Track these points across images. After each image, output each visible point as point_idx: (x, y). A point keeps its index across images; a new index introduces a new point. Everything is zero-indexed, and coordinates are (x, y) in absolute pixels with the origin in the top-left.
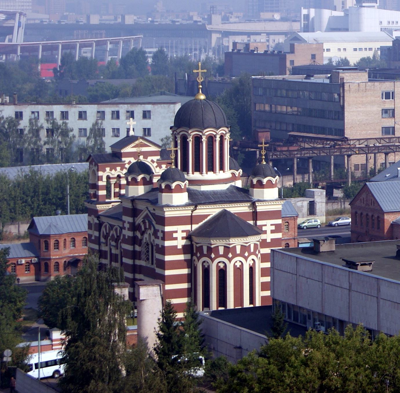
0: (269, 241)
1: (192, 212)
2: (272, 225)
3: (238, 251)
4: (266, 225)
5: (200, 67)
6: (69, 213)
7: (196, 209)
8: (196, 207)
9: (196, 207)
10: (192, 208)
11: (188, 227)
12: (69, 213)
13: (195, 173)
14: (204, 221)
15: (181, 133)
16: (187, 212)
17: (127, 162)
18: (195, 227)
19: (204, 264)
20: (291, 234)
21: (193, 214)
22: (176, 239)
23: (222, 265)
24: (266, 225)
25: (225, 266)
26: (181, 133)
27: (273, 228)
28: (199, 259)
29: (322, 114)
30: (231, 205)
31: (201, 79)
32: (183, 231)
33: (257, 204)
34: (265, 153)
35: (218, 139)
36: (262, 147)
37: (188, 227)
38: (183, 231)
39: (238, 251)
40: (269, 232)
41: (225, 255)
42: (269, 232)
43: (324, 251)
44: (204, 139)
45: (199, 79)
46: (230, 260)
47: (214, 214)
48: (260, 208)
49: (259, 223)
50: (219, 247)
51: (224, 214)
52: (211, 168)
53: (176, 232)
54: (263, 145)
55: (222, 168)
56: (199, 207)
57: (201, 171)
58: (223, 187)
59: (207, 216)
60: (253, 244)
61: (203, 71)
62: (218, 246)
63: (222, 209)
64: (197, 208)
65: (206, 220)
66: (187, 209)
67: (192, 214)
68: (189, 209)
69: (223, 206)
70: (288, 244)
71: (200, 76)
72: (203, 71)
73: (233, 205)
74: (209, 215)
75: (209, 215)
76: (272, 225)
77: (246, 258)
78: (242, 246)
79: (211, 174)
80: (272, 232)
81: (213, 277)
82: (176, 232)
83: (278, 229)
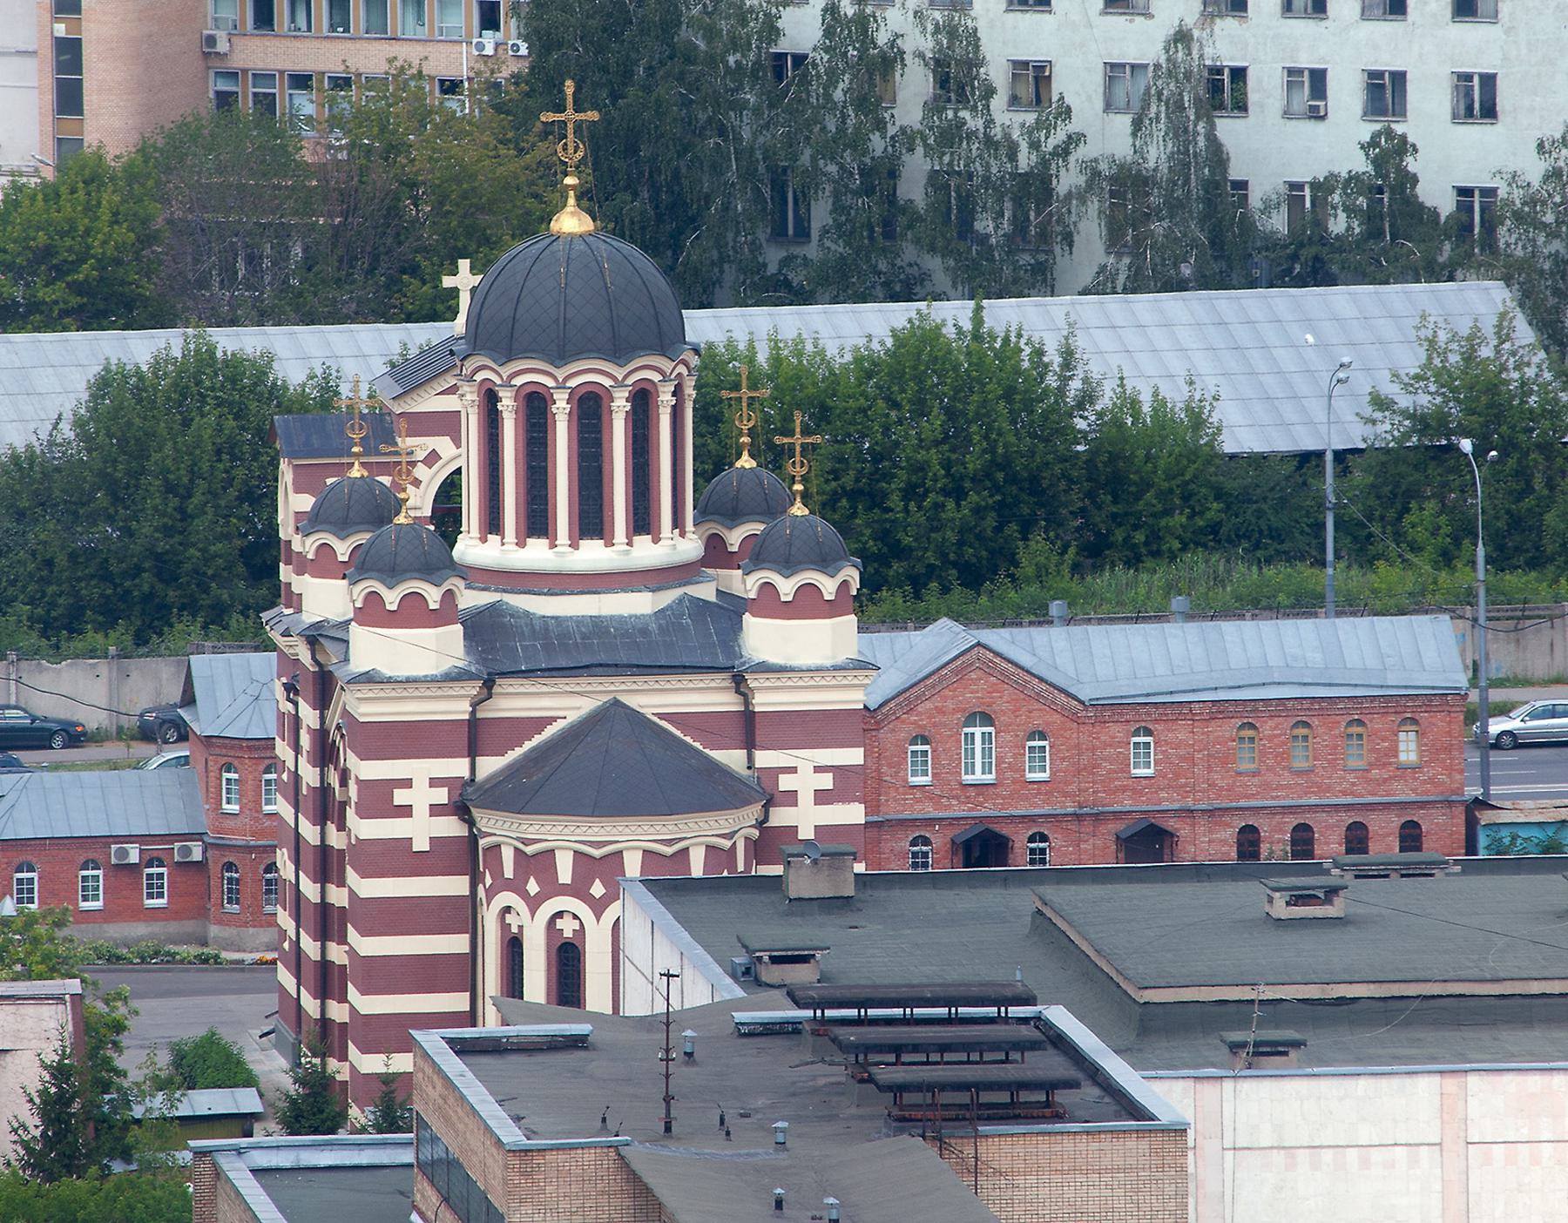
0: (807, 833)
1: (475, 705)
2: (818, 769)
3: (565, 875)
4: (793, 770)
5: (570, 100)
6: (1329, 457)
7: (490, 696)
8: (490, 688)
9: (489, 684)
10: (473, 689)
11: (458, 767)
12: (1329, 457)
13: (584, 543)
14: (528, 745)
15: (479, 377)
16: (455, 707)
17: (420, 455)
18: (489, 765)
19: (509, 918)
20: (1431, 780)
21: (479, 715)
22: (406, 811)
23: (567, 927)
24: (793, 770)
25: (581, 932)
26: (479, 377)
27: (826, 782)
28: (534, 904)
29: (1053, 287)
30: (641, 682)
31: (576, 149)
32: (435, 782)
33: (752, 684)
34: (805, 470)
35: (620, 405)
36: (791, 447)
37: (458, 767)
38: (435, 782)
39: (565, 875)
40: (806, 798)
41: (578, 889)
42: (806, 798)
43: (806, 896)
44: (561, 407)
45: (565, 149)
46: (599, 907)
47: (573, 717)
48: (767, 700)
49: (764, 759)
50: (625, 854)
51: (614, 712)
52: (591, 523)
53: (407, 783)
54: (798, 440)
55: (643, 522)
56: (504, 686)
57: (606, 531)
58: (639, 604)
59: (541, 723)
60: (702, 850)
61: (581, 116)
62: (552, 851)
63: (605, 698)
64: (496, 689)
65: (537, 740)
66: (451, 692)
67: (473, 713)
68: (462, 692)
69: (612, 688)
70: (1416, 825)
71: (571, 136)
72: (581, 116)
73: (651, 681)
74: (554, 719)
75: (554, 719)
76: (818, 769)
77: (599, 907)
78: (709, 848)
79: (643, 541)
80: (822, 797)
81: (493, 962)
82: (407, 783)
83: (845, 785)
